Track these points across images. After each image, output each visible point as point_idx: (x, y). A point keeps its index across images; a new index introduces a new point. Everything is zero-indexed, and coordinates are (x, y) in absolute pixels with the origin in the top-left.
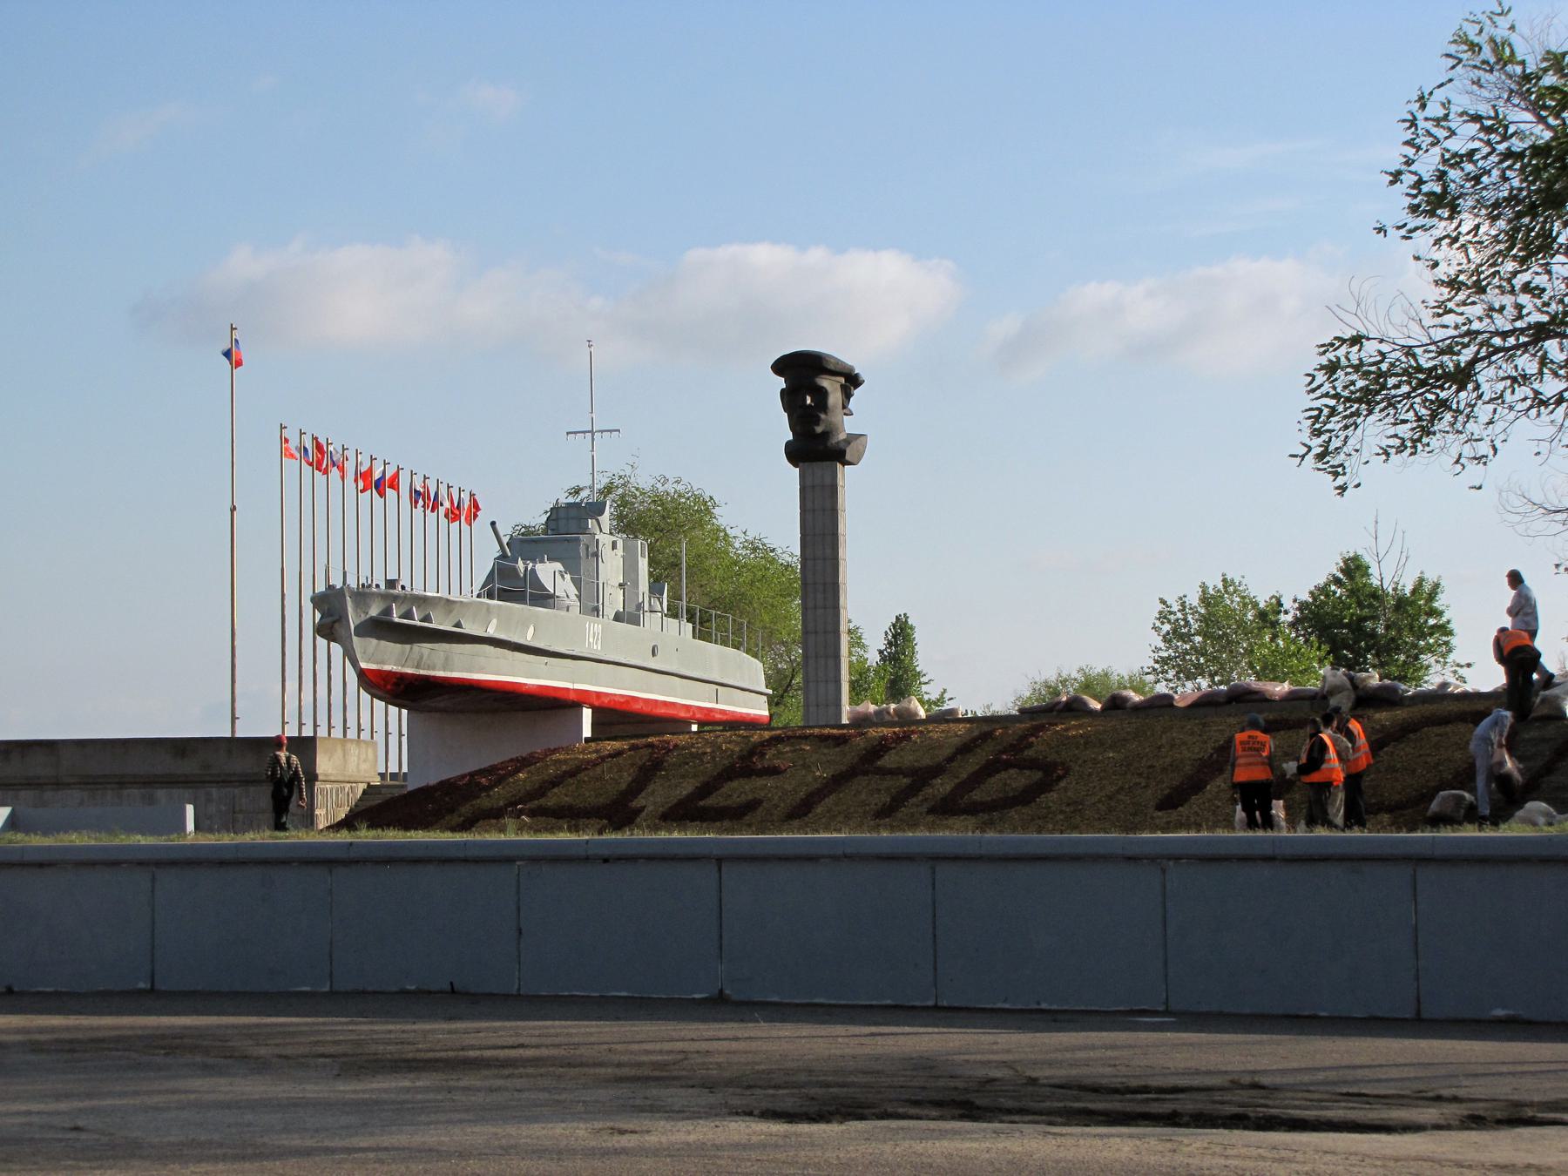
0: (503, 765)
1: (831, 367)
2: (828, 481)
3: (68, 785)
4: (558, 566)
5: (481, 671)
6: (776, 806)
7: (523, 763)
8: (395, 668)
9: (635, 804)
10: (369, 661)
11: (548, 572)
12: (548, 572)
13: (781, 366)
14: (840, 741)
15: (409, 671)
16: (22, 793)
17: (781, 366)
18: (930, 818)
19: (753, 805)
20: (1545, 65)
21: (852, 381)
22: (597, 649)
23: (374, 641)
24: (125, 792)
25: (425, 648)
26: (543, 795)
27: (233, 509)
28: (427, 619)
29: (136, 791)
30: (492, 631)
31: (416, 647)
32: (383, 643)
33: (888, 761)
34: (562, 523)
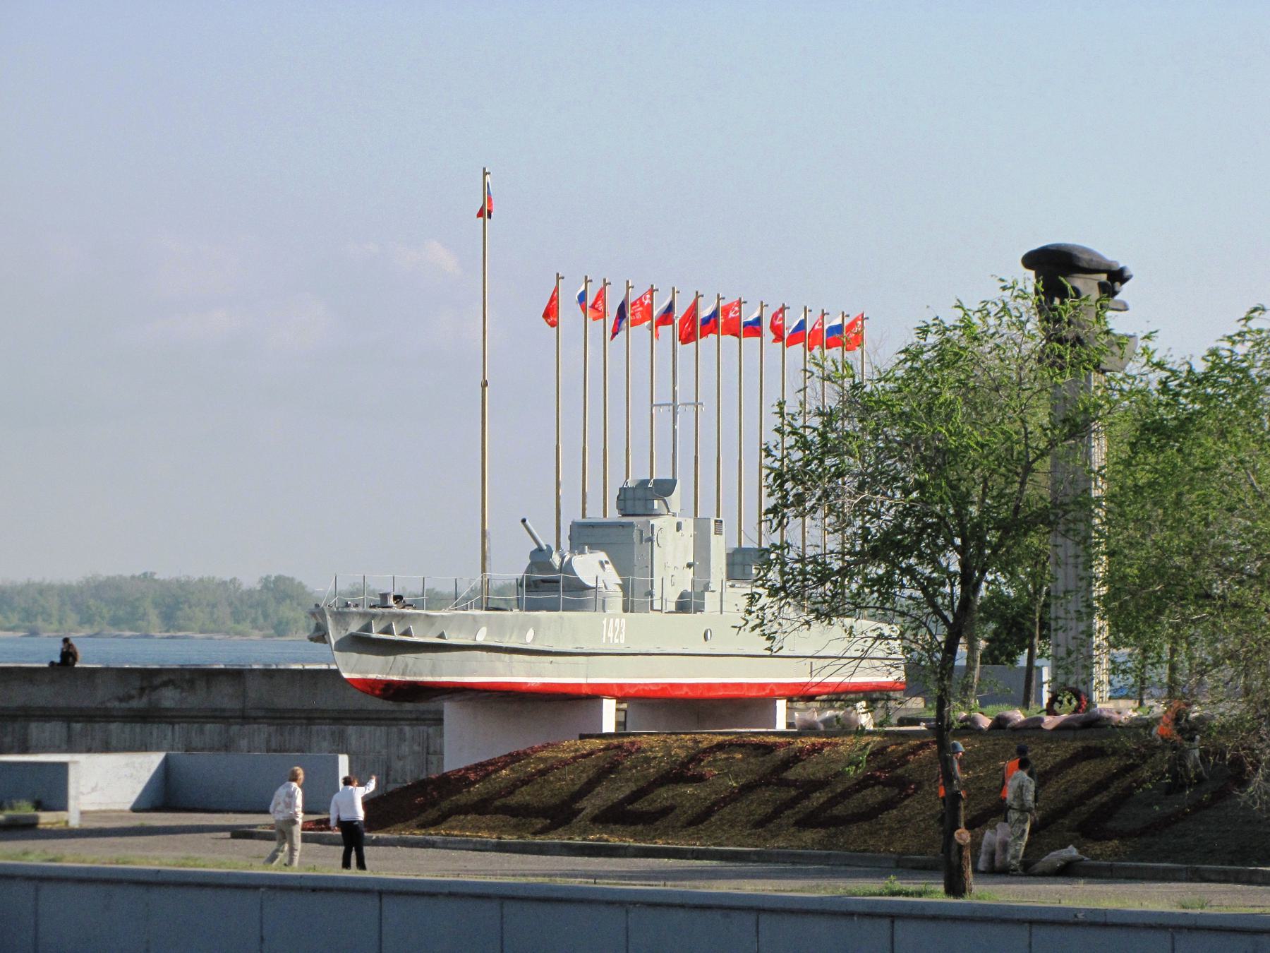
0: (490, 763)
1: (1084, 265)
2: (114, 743)
3: (255, 719)
4: (603, 556)
5: (472, 674)
6: (685, 812)
7: (514, 758)
8: (380, 677)
9: (578, 806)
10: (351, 672)
11: (591, 567)
12: (591, 567)
13: (1031, 260)
14: (768, 749)
15: (395, 678)
16: (208, 727)
17: (1031, 260)
18: (792, 830)
19: (665, 811)
20: (958, 323)
21: (1118, 276)
22: (619, 643)
23: (355, 655)
24: (315, 728)
25: (410, 658)
26: (511, 793)
27: (485, 384)
28: (407, 633)
29: (327, 728)
30: (481, 638)
31: (400, 657)
32: (364, 656)
33: (791, 774)
34: (629, 503)
